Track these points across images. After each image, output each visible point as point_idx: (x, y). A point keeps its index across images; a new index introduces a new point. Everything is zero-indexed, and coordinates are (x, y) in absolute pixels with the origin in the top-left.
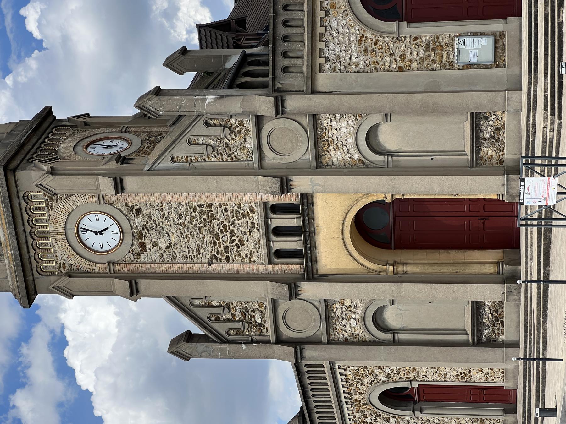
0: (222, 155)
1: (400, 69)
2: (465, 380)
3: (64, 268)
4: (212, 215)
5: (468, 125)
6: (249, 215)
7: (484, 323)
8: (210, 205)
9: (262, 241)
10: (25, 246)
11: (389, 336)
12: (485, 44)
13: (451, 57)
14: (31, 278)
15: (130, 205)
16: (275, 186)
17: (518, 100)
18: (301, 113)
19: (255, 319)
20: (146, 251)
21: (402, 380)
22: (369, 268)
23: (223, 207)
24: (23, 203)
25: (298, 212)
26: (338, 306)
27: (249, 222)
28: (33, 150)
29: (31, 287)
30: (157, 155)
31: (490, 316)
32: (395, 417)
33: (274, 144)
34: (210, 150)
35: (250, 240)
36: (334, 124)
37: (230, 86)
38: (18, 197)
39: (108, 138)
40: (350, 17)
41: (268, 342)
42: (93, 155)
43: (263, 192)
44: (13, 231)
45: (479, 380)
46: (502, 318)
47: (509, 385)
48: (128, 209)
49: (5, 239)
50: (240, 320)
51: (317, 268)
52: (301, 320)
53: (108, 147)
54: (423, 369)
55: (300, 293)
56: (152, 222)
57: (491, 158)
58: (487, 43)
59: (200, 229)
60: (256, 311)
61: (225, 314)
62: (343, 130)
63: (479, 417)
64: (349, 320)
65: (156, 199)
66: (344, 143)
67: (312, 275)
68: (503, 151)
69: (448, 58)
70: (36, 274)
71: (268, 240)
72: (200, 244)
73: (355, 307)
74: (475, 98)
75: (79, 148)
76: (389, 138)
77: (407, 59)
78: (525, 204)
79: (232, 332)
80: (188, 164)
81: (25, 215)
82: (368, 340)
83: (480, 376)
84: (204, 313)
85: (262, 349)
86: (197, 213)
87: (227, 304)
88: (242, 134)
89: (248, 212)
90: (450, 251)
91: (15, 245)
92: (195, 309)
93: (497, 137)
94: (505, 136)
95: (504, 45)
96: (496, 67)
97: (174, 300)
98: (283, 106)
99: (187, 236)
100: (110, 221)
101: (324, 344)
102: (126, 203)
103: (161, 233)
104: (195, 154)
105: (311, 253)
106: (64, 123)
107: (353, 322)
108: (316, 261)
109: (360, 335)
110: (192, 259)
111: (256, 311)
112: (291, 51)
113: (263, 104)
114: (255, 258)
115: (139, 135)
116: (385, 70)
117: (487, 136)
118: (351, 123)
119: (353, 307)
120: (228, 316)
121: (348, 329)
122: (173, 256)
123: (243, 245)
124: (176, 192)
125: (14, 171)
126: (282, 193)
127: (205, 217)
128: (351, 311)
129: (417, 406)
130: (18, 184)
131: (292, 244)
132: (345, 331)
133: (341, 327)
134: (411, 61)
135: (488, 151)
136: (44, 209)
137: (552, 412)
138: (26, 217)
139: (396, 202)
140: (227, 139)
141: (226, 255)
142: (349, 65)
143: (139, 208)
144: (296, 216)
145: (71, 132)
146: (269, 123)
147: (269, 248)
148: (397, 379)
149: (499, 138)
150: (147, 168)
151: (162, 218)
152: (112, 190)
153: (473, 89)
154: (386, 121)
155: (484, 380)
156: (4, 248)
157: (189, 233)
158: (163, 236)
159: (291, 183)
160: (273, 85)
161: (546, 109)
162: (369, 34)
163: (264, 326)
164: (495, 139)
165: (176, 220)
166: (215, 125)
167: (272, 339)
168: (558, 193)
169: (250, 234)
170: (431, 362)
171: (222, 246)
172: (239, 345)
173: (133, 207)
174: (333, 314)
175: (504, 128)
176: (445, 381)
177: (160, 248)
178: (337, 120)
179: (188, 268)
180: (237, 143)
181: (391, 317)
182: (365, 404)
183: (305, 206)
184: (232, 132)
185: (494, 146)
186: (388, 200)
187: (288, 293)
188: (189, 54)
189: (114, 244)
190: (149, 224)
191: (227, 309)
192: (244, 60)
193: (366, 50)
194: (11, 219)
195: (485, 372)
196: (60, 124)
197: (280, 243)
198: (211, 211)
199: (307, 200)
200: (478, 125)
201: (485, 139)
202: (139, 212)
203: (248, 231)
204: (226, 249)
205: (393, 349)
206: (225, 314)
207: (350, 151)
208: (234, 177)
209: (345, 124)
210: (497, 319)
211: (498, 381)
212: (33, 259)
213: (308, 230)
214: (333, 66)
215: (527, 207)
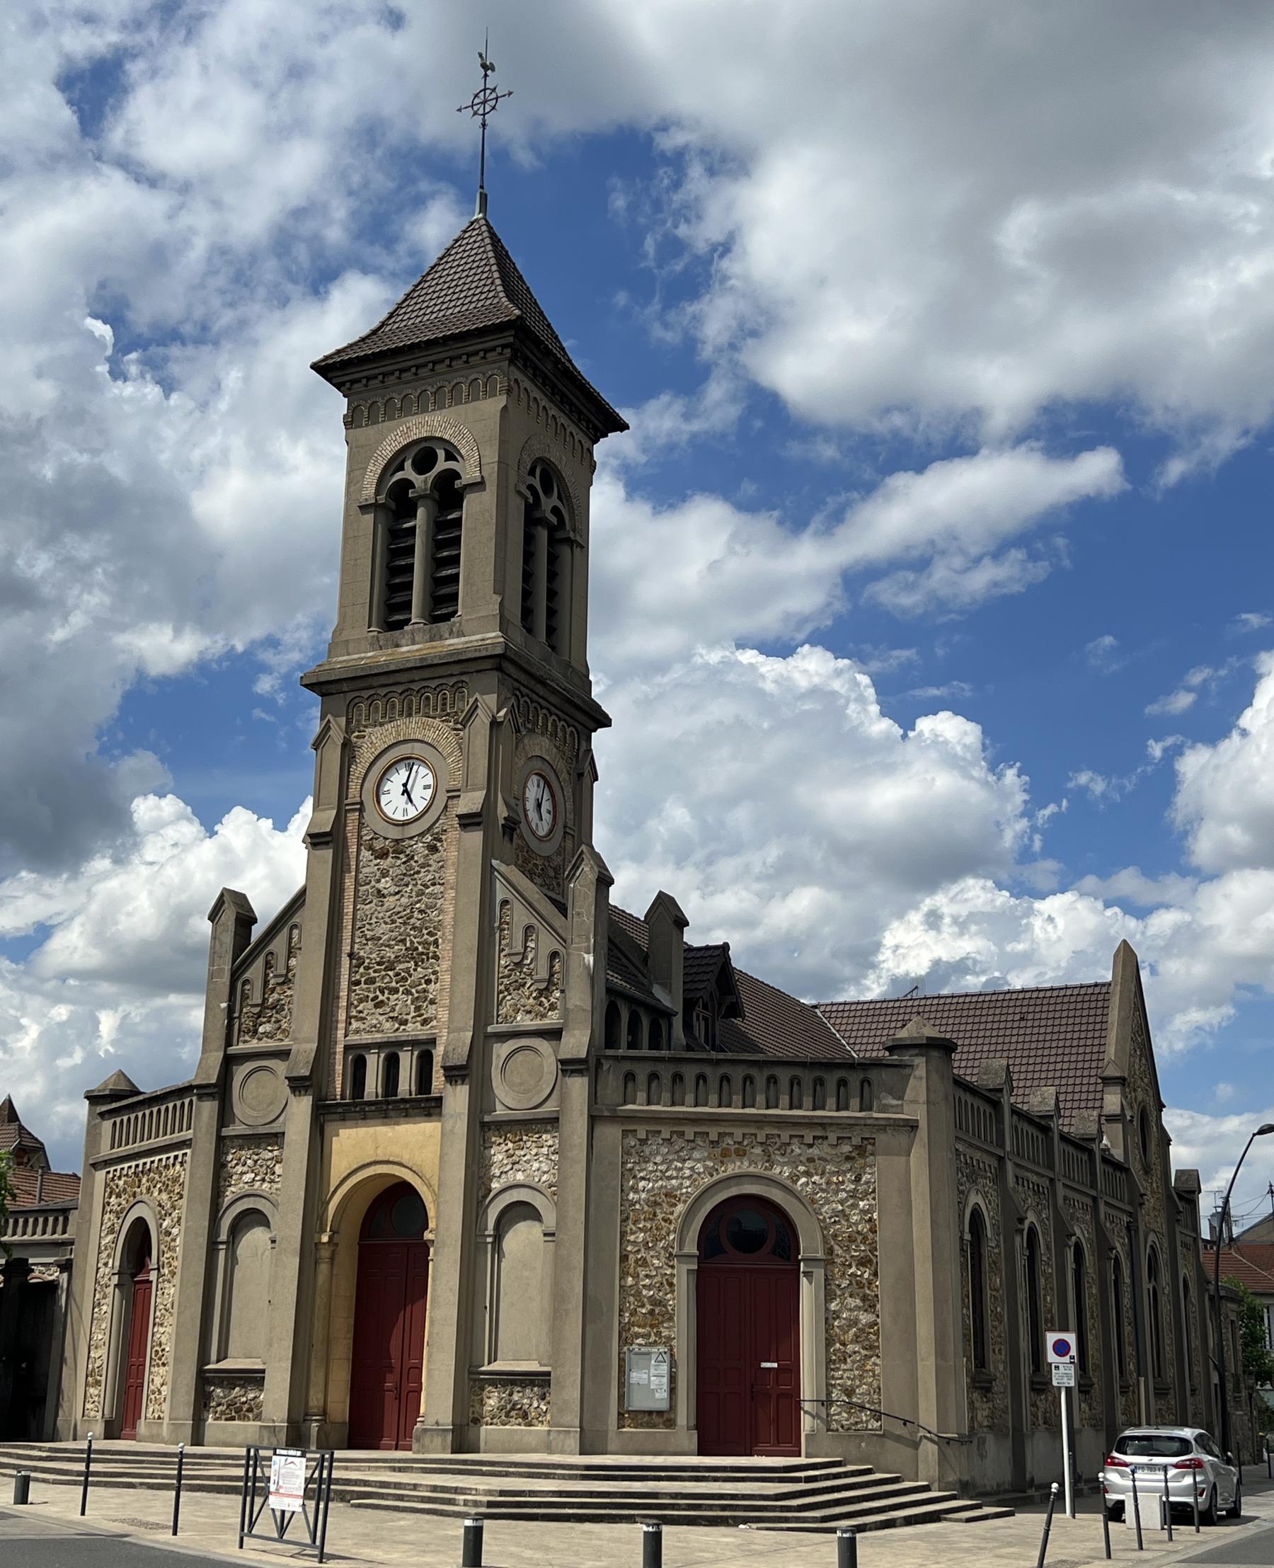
0: (509, 976)
1: (624, 1258)
3: (357, 737)
4: (423, 961)
5: (533, 1366)
8: (436, 957)
9: (380, 1035)
10: (391, 681)
11: (223, 1236)
12: (657, 1395)
13: (640, 1341)
18: (563, 1100)
22: (328, 1203)
23: (433, 977)
24: (454, 680)
25: (419, 1092)
27: (409, 1017)
28: (535, 697)
29: (333, 688)
30: (512, 879)
31: (244, 1399)
33: (519, 1057)
34: (517, 959)
35: (381, 1018)
36: (545, 1150)
37: (610, 991)
38: (462, 674)
39: (554, 807)
40: (708, 1180)
41: (229, 1043)
42: (526, 783)
43: (452, 1041)
44: (411, 665)
46: (240, 1419)
47: (142, 1427)
49: (403, 653)
50: (265, 1000)
52: (262, 1096)
53: (539, 805)
57: (482, 1404)
58: (660, 1398)
59: (403, 941)
62: (536, 1165)
63: (103, 1378)
65: (450, 875)
66: (516, 1167)
67: (325, 1116)
69: (638, 1336)
70: (351, 695)
71: (380, 1046)
73: (272, 1181)
75: (538, 764)
76: (521, 1237)
77: (639, 1269)
78: (274, 1458)
79: (247, 987)
80: (497, 924)
81: (437, 682)
83: (158, 1381)
84: (278, 945)
85: (221, 1033)
90: (351, 1335)
91: (393, 668)
92: (286, 931)
93: (513, 1413)
95: (654, 1426)
96: (619, 1414)
97: (298, 901)
98: (573, 1071)
99: (393, 922)
100: (421, 805)
101: (219, 1131)
103: (400, 882)
106: (584, 744)
107: (248, 1177)
108: (344, 1120)
112: (660, 1085)
113: (577, 1042)
114: (355, 1025)
115: (558, 853)
116: (623, 1234)
117: (516, 1397)
123: (376, 1006)
124: (456, 906)
125: (499, 669)
126: (445, 1068)
129: (127, 1277)
131: (373, 1085)
134: (636, 1276)
136: (443, 710)
137: (22, 1497)
138: (433, 684)
139: (425, 1247)
142: (635, 1177)
144: (413, 1089)
145: (568, 754)
147: (368, 1047)
148: (162, 1247)
150: (494, 862)
153: (587, 1376)
154: (545, 1235)
155: (152, 1387)
156: (390, 651)
160: (607, 1057)
161: (502, 1493)
162: (680, 1208)
163: (253, 1037)
164: (511, 1411)
167: (233, 1050)
168: (283, 1512)
172: (226, 997)
173: (440, 840)
174: (263, 1145)
177: (378, 881)
181: (255, 1238)
182: (134, 1195)
183: (426, 1105)
184: (541, 992)
185: (501, 1409)
186: (428, 1236)
188: (675, 931)
189: (388, 810)
191: (282, 980)
192: (661, 1015)
194: (429, 662)
196: (583, 737)
197: (374, 1064)
199: (428, 1106)
201: (511, 1394)
202: (433, 849)
204: (371, 981)
211: (149, 1411)
212: (372, 692)
214: (633, 1151)
215: (270, 1459)
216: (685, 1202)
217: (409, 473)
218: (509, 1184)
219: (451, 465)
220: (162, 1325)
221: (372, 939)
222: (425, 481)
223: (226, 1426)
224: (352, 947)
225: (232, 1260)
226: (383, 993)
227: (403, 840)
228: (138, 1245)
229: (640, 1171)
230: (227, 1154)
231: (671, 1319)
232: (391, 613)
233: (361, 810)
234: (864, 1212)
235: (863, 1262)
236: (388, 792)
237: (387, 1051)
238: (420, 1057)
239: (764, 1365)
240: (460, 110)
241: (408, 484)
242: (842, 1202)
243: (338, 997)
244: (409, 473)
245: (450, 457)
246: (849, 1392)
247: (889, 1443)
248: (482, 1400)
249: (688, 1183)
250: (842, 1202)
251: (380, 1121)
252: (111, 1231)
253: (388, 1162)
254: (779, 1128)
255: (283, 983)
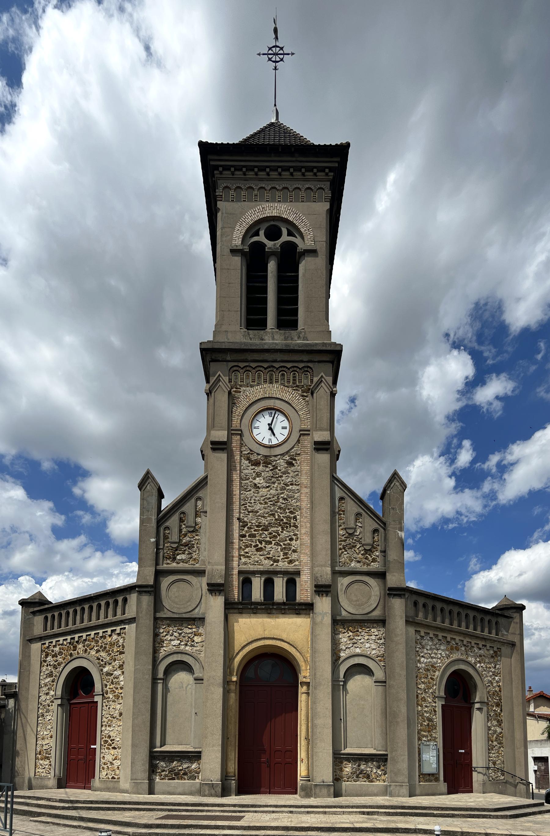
2: (102, 743)
3: (235, 392)
6: (286, 558)
7: (173, 762)
11: (161, 675)
13: (424, 739)
14: (229, 358)
15: (296, 458)
16: (323, 580)
17: (401, 794)
19: (180, 554)
20: (252, 465)
21: (104, 686)
22: (234, 659)
23: (294, 537)
26: (194, 630)
31: (181, 768)
32: (53, 682)
33: (355, 586)
34: (350, 531)
35: (262, 557)
41: (157, 564)
45: (104, 757)
46: (178, 779)
47: (96, 783)
48: (293, 455)
51: (234, 613)
52: (177, 596)
54: (119, 705)
55: (213, 594)
56: (280, 474)
59: (273, 515)
60: (190, 556)
61: (187, 527)
62: (368, 645)
64: (178, 640)
67: (231, 607)
68: (348, 781)
71: (262, 573)
72: (259, 514)
73: (192, 646)
74: (402, 757)
77: (423, 703)
80: (337, 510)
82: (157, 655)
86: (288, 514)
87: (197, 530)
88: (364, 560)
89: (289, 558)
92: (193, 500)
93: (360, 776)
94: (362, 783)
95: (431, 781)
98: (395, 595)
99: (266, 503)
100: (281, 438)
102: (299, 454)
103: (269, 481)
104: (347, 518)
105: (250, 609)
107: (176, 642)
108: (241, 613)
109: (162, 648)
110: (243, 505)
111: (190, 556)
114: (243, 560)
117: (362, 767)
118: (374, 652)
119: (193, 643)
120: (184, 530)
121: (168, 637)
122: (246, 489)
123: (258, 550)
127: (285, 520)
128: (188, 641)
129: (65, 701)
130: (320, 364)
131: (257, 594)
132: (167, 635)
133: (171, 631)
134: (421, 706)
135: (348, 768)
140: (360, 547)
141: (247, 534)
142: (419, 655)
143: (293, 465)
146: (376, 584)
147: (254, 573)
149: (360, 778)
151: (283, 484)
152: (316, 439)
157: (269, 505)
158: (266, 482)
159: (324, 595)
164: (358, 774)
165: (282, 495)
166: (374, 538)
167: (160, 567)
169: (268, 558)
170: (133, 712)
171: (256, 533)
172: (154, 534)
173: (295, 460)
174: (185, 625)
175: (369, 782)
176: (102, 726)
177: (255, 479)
178: (377, 641)
179: (236, 499)
180: (355, 555)
181: (181, 678)
183: (294, 607)
187: (215, 582)
190: (278, 472)
191: (192, 529)
193: (428, 670)
195: (114, 762)
197: (257, 585)
198: (290, 526)
199: (307, 608)
200: (372, 760)
201: (359, 766)
202: (290, 464)
203: (270, 556)
204: (254, 536)
205: (148, 677)
206: (187, 527)
207: (348, 650)
208: (329, 546)
209: (373, 646)
210: (177, 774)
213: (275, 607)
216: (439, 670)
217: (262, 238)
218: (351, 654)
219: (291, 239)
220: (109, 726)
221: (252, 512)
222: (275, 245)
223: (170, 783)
224: (240, 515)
225: (166, 690)
226: (261, 543)
227: (270, 456)
228: (79, 684)
229: (421, 652)
230: (159, 628)
231: (435, 728)
232: (254, 318)
233: (241, 435)
234: (497, 682)
235: (498, 705)
236: (257, 428)
237: (266, 576)
238: (287, 582)
239: (460, 751)
240: (259, 54)
241: (260, 246)
242: (491, 676)
243: (233, 543)
244: (262, 238)
245: (290, 234)
246: (494, 763)
247: (508, 786)
248: (341, 769)
249: (439, 661)
250: (491, 676)
251: (265, 615)
252: (50, 675)
253: (273, 639)
254: (471, 639)
255: (193, 531)
